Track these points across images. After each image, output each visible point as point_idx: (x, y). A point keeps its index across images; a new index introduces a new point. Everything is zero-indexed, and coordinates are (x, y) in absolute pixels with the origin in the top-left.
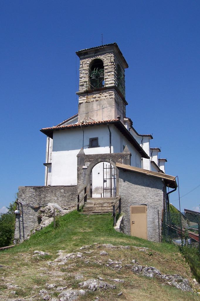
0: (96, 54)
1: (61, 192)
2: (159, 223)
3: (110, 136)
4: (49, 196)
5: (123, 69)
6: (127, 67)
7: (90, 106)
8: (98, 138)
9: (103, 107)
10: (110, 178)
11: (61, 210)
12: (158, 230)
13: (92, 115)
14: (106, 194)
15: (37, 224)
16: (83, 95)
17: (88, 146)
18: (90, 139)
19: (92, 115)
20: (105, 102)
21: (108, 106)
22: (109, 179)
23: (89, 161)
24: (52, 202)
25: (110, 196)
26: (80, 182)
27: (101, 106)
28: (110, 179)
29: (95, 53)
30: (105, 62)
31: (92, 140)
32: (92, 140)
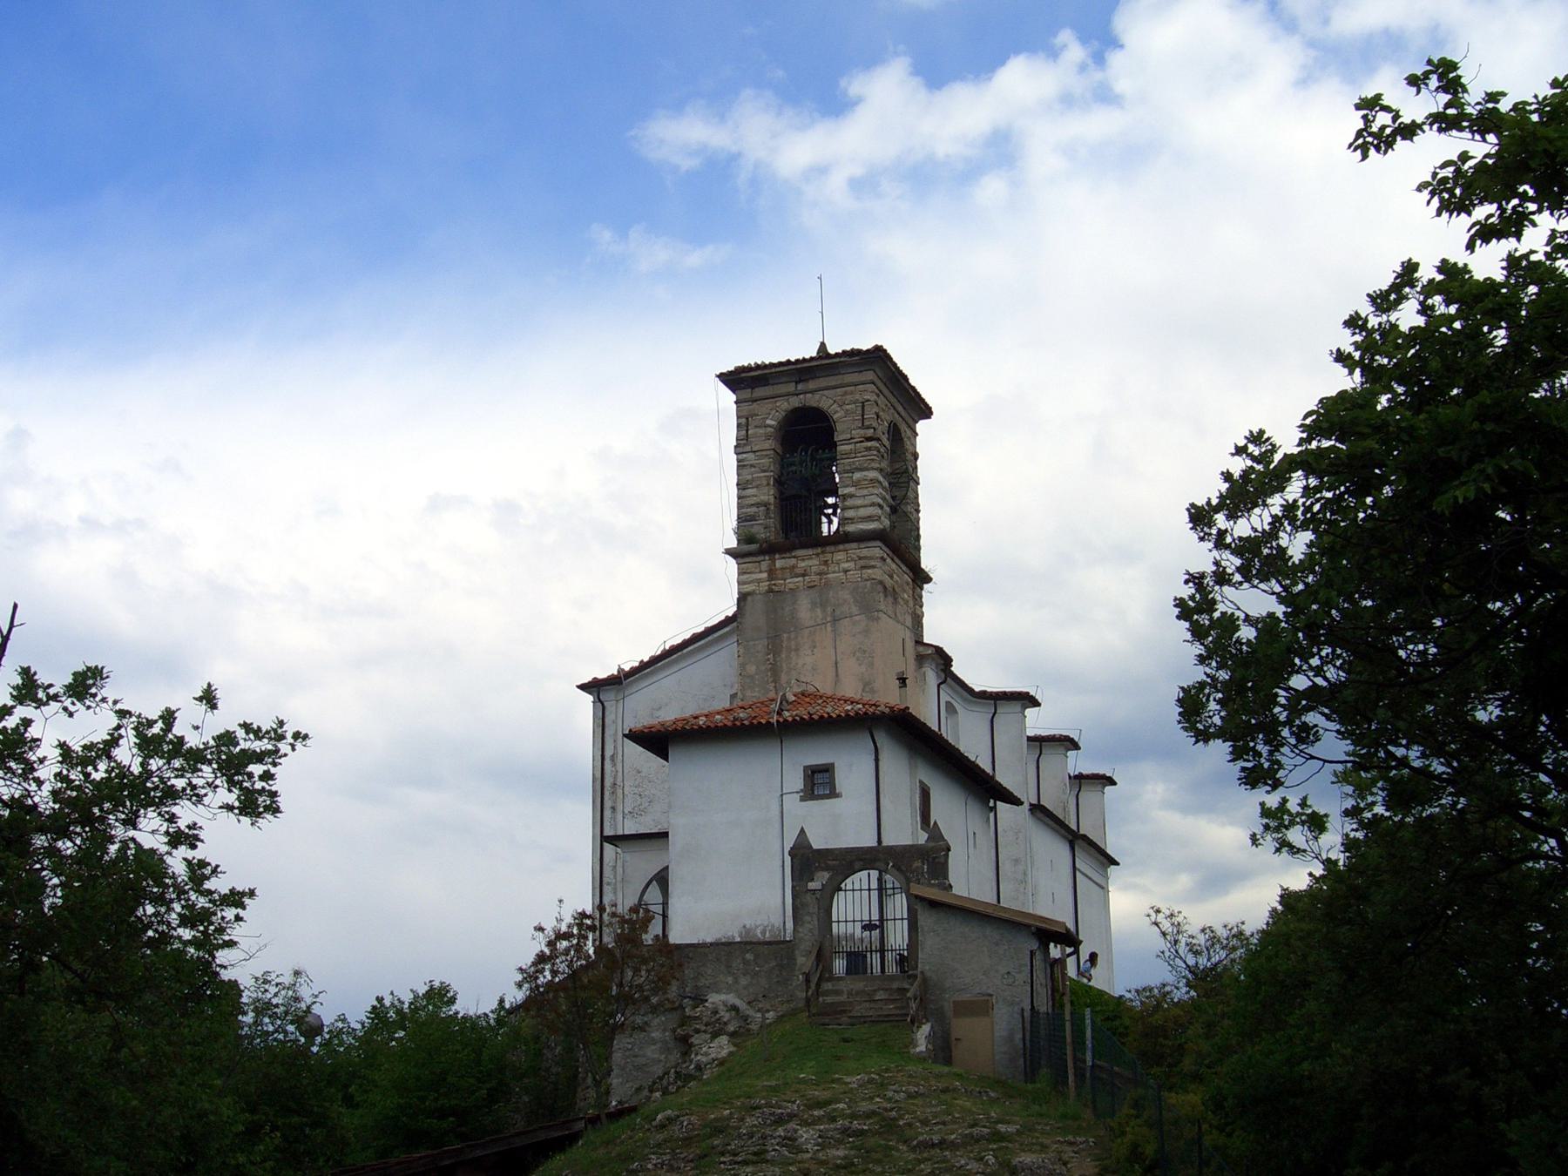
0: (800, 387)
1: (746, 962)
2: (1024, 1044)
3: (877, 760)
4: (709, 972)
5: (909, 427)
6: (926, 412)
7: (783, 609)
8: (833, 765)
9: (838, 612)
10: (885, 922)
11: (748, 1012)
12: (1021, 1061)
13: (793, 647)
14: (874, 961)
15: (675, 1057)
16: (754, 559)
17: (797, 792)
18: (806, 768)
19: (793, 647)
20: (845, 595)
21: (855, 610)
22: (887, 920)
23: (827, 869)
24: (718, 992)
25: (879, 971)
26: (800, 930)
27: (829, 609)
28: (885, 918)
29: (797, 383)
30: (839, 427)
31: (813, 772)
32: (813, 772)
